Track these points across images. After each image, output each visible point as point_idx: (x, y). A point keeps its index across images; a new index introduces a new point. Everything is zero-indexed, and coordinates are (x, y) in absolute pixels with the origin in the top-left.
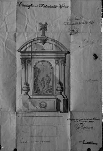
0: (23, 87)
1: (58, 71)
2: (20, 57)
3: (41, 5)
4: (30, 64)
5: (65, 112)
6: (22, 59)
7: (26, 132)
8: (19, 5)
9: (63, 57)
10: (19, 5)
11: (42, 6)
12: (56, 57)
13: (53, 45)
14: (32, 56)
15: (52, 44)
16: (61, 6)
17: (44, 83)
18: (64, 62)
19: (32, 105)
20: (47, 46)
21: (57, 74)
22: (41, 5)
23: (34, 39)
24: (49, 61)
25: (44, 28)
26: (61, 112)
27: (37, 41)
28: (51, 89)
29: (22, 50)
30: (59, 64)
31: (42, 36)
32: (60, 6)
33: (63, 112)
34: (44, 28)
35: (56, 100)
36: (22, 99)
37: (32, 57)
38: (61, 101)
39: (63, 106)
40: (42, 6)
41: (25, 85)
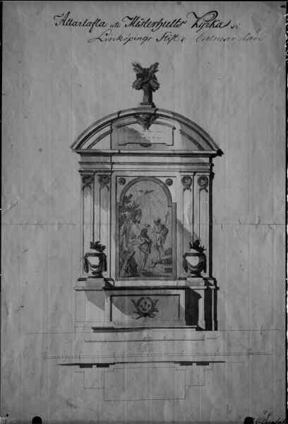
0: (187, 254)
1: (186, 203)
2: (79, 167)
3: (130, 21)
4: (108, 187)
5: (208, 327)
6: (85, 171)
7: (173, 399)
8: (64, 21)
9: (205, 167)
10: (64, 21)
11: (132, 24)
12: (186, 164)
13: (177, 132)
14: (113, 163)
15: (174, 128)
16: (199, 24)
17: (149, 243)
18: (207, 182)
19: (113, 306)
20: (158, 134)
21: (184, 214)
22: (130, 21)
23: (120, 112)
24: (160, 178)
25: (146, 80)
26: (199, 329)
27: (126, 120)
28: (169, 262)
29: (85, 146)
30: (191, 187)
31: (141, 104)
32: (196, 24)
33: (204, 328)
34: (146, 80)
35: (182, 293)
36: (85, 290)
37: (114, 166)
38: (199, 297)
39: (201, 311)
40: (134, 22)
41: (191, 248)
